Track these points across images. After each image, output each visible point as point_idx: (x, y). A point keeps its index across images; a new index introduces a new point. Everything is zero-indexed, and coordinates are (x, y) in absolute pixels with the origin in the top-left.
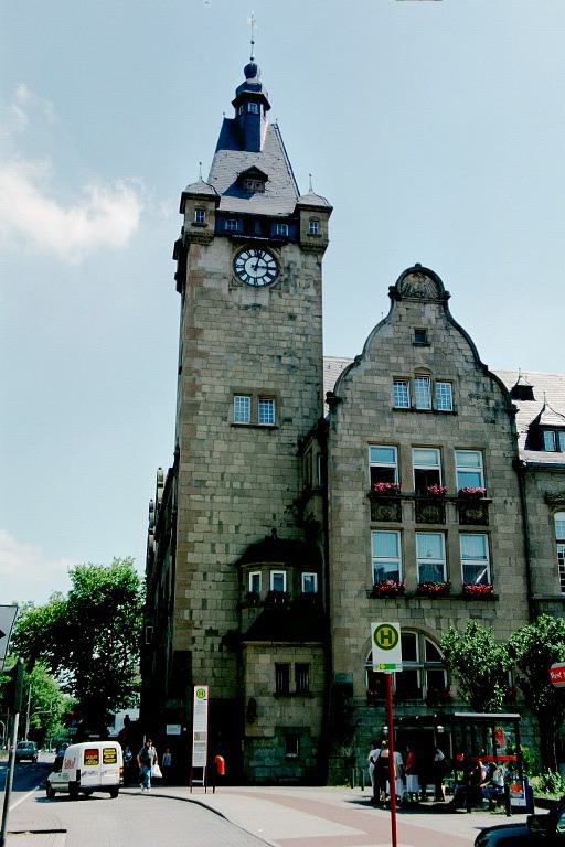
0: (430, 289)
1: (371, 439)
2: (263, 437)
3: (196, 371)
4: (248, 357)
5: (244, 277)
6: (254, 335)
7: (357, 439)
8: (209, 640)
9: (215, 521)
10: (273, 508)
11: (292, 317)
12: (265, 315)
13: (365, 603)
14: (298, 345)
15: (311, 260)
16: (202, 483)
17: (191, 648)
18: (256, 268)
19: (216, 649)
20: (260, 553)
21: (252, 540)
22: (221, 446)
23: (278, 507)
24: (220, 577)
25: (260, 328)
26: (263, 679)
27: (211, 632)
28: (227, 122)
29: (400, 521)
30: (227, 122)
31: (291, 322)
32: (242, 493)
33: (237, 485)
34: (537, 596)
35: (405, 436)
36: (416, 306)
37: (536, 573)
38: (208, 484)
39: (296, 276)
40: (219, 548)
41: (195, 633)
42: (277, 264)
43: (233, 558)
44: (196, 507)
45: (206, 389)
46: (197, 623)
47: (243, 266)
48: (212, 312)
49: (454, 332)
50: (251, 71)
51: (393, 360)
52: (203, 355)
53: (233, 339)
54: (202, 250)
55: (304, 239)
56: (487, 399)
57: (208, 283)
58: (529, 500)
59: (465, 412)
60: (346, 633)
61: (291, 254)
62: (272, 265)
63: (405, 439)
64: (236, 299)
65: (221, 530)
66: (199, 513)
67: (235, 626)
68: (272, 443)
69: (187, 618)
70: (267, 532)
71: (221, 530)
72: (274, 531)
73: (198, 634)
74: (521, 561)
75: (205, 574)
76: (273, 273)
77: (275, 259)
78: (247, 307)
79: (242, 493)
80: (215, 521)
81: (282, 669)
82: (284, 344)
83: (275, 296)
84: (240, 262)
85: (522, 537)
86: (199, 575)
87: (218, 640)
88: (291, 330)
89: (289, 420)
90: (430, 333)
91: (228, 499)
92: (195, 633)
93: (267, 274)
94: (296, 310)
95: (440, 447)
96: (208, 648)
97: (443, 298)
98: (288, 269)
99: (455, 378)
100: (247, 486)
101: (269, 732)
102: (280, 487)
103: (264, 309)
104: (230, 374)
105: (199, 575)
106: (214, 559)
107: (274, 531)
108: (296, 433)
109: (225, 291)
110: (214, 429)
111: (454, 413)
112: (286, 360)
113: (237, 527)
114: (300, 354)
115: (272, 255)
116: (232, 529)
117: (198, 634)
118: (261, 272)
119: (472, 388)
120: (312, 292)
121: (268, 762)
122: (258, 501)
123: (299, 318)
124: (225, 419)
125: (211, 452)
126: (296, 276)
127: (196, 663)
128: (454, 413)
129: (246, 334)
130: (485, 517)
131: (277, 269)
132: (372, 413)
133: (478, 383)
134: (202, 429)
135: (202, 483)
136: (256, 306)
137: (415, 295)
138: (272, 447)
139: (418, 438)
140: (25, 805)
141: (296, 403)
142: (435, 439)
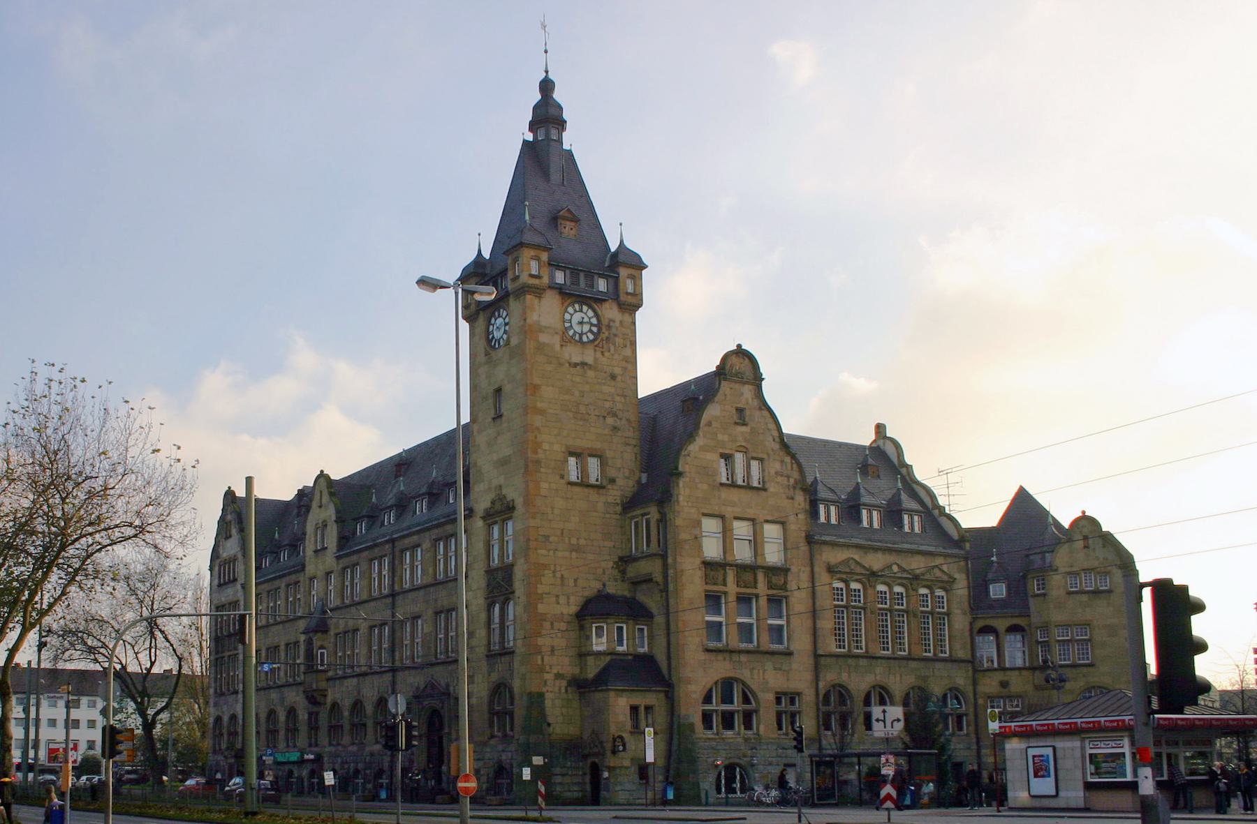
0: (749, 373)
1: (705, 511)
2: (593, 495)
3: (538, 429)
4: (579, 416)
5: (571, 333)
6: (582, 394)
7: (693, 510)
8: (557, 682)
9: (558, 575)
10: (603, 564)
11: (613, 377)
12: (591, 373)
13: (703, 656)
14: (619, 406)
15: (627, 318)
16: (547, 537)
17: (544, 690)
18: (581, 323)
19: (563, 690)
20: (595, 608)
21: (588, 593)
22: (560, 503)
23: (608, 564)
24: (563, 626)
25: (587, 388)
26: (621, 718)
27: (558, 676)
28: (525, 143)
29: (725, 585)
30: (525, 143)
31: (613, 383)
32: (577, 549)
33: (574, 541)
34: (820, 652)
35: (729, 509)
36: (737, 386)
37: (819, 633)
38: (551, 539)
39: (615, 335)
40: (562, 600)
41: (547, 676)
42: (599, 320)
43: (573, 609)
44: (543, 560)
45: (546, 446)
46: (547, 668)
47: (570, 321)
48: (549, 368)
49: (766, 413)
50: (546, 86)
51: (720, 437)
52: (542, 412)
53: (566, 397)
54: (536, 301)
55: (623, 298)
56: (788, 477)
57: (544, 338)
58: (817, 569)
59: (772, 488)
60: (689, 682)
61: (610, 311)
62: (594, 321)
63: (729, 511)
64: (567, 357)
65: (562, 584)
66: (545, 566)
67: (577, 671)
68: (600, 500)
69: (539, 662)
70: (596, 585)
71: (562, 584)
72: (604, 585)
73: (549, 677)
74: (809, 623)
75: (552, 624)
76: (595, 329)
77: (597, 315)
78: (576, 365)
79: (577, 549)
80: (558, 575)
81: (634, 709)
82: (607, 405)
83: (599, 355)
84: (567, 316)
85: (810, 601)
86: (547, 625)
87: (564, 683)
88: (612, 390)
89: (612, 481)
90: (748, 413)
91: (567, 554)
92: (547, 676)
93: (591, 331)
94: (617, 371)
95: (753, 520)
96: (557, 689)
97: (757, 379)
98: (609, 327)
99: (765, 456)
100: (582, 542)
101: (627, 763)
102: (608, 544)
103: (590, 366)
104: (565, 433)
105: (547, 625)
106: (558, 610)
107: (604, 585)
108: (619, 493)
109: (558, 347)
110: (554, 486)
111: (764, 489)
112: (610, 421)
113: (575, 581)
114: (620, 414)
115: (594, 311)
116: (571, 583)
117: (549, 677)
118: (586, 328)
119: (777, 466)
120: (628, 352)
121: (628, 786)
122: (590, 557)
123: (619, 378)
124: (562, 477)
125: (552, 508)
126: (615, 335)
127: (548, 703)
128: (764, 489)
129: (577, 394)
130: (785, 583)
131: (599, 325)
132: (705, 487)
133: (782, 462)
134: (544, 485)
135: (547, 537)
136: (584, 364)
137: (736, 375)
138: (600, 506)
139: (738, 511)
140: (1219, 668)
141: (619, 462)
142: (750, 513)
